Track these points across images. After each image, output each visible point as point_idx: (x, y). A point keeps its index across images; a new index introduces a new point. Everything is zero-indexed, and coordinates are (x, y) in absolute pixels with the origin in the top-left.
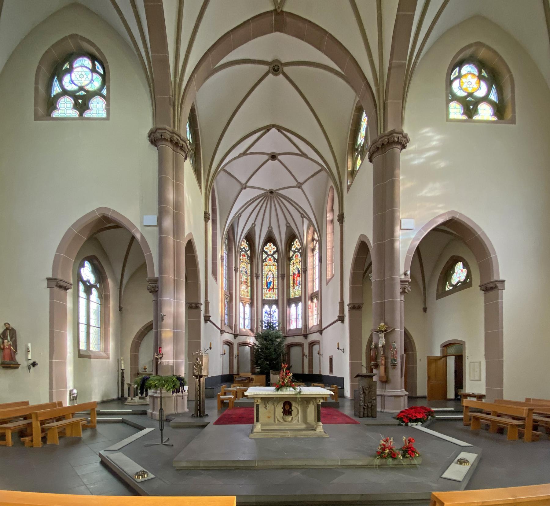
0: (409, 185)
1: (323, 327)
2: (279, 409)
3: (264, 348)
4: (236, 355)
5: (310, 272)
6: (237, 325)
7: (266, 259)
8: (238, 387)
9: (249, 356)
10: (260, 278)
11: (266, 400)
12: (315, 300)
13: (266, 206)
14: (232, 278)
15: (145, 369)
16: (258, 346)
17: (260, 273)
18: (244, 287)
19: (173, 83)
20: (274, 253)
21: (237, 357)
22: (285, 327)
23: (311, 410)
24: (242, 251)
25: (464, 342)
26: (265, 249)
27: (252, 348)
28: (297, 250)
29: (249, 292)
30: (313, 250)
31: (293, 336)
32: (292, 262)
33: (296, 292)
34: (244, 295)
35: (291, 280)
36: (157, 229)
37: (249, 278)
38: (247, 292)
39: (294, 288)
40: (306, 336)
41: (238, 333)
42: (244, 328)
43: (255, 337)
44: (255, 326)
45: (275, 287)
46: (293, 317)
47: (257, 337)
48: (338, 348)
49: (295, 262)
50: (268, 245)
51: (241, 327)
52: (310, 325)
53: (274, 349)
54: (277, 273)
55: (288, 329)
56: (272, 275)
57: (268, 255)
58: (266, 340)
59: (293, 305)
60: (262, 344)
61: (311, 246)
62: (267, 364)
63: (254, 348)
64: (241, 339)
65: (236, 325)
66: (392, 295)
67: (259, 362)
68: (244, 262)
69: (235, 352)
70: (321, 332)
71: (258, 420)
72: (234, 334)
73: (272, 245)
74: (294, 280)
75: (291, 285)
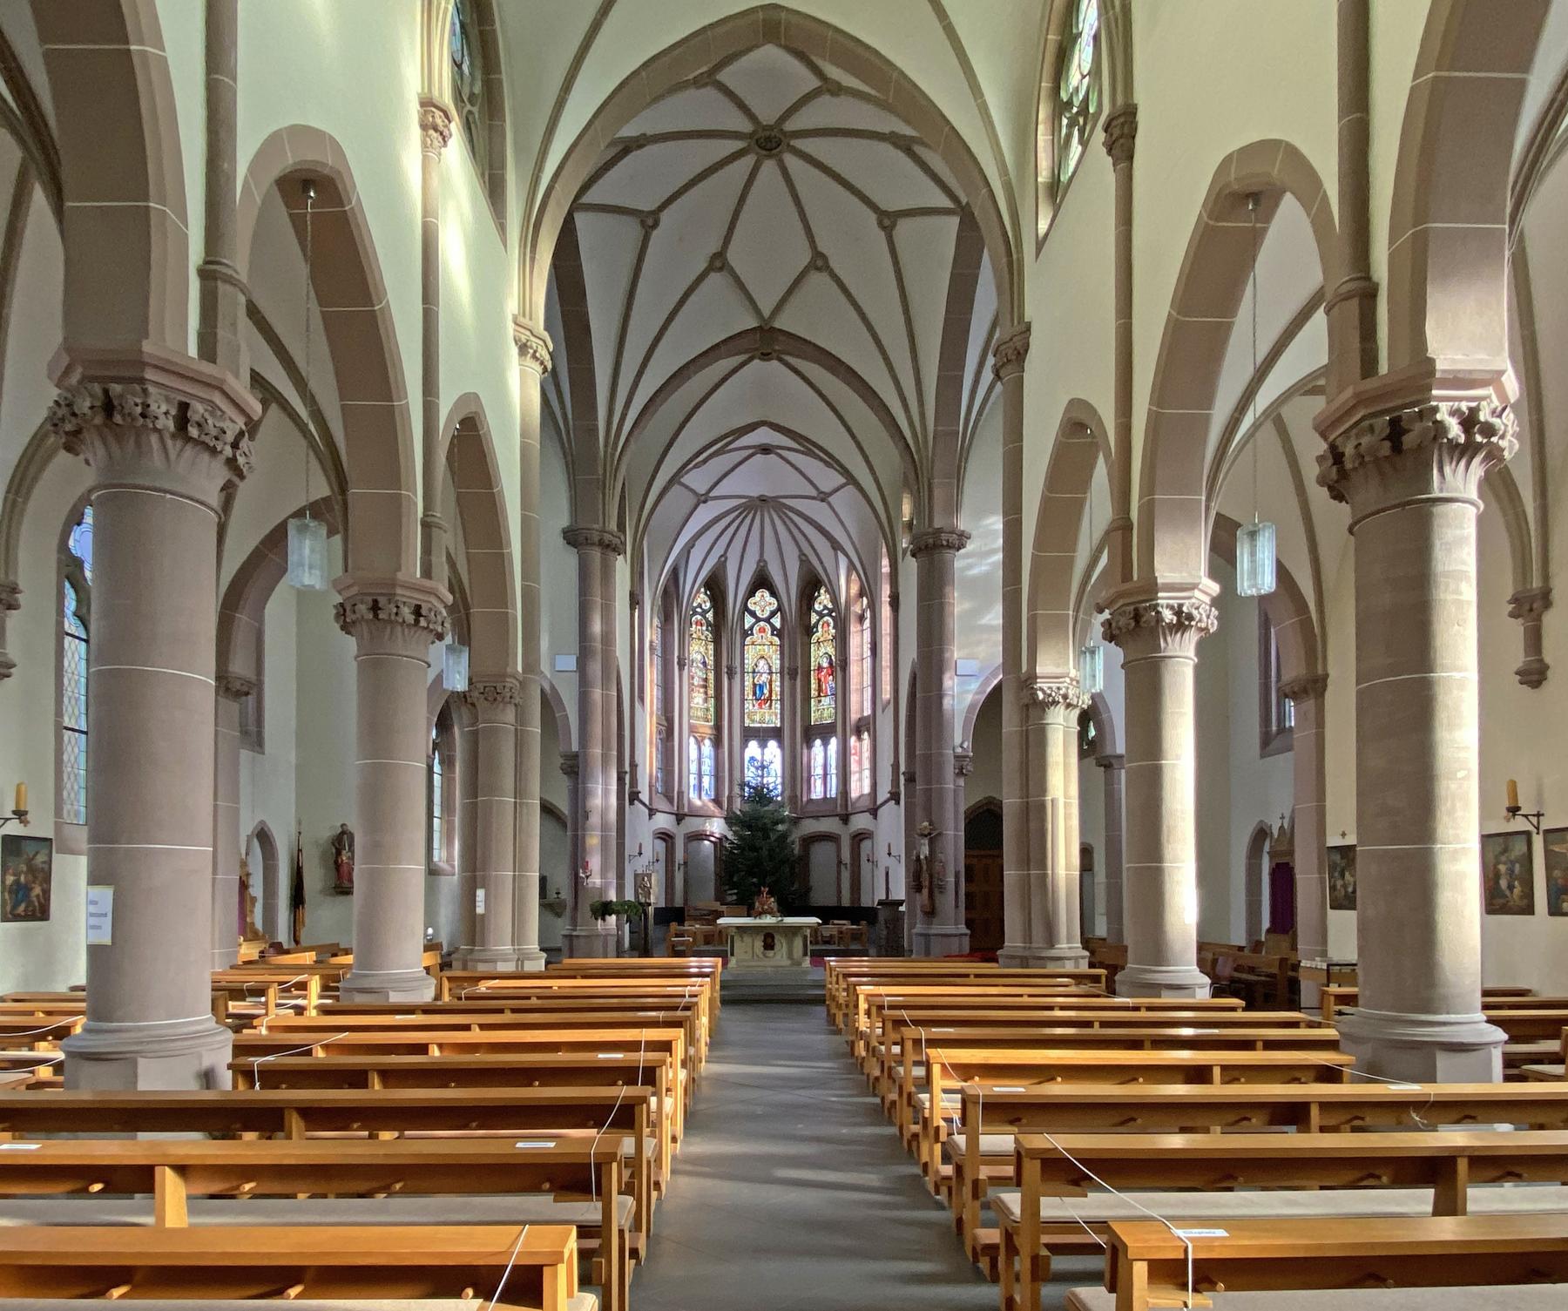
0: (967, 605)
1: (879, 802)
2: (759, 944)
3: (746, 846)
4: (682, 862)
5: (854, 669)
6: (683, 792)
7: (751, 628)
8: (697, 926)
9: (712, 868)
10: (737, 678)
11: (742, 929)
12: (866, 736)
13: (753, 521)
14: (673, 683)
15: (558, 893)
16: (733, 843)
17: (737, 663)
18: (698, 698)
19: (602, 453)
20: (773, 614)
21: (682, 868)
22: (799, 794)
23: (798, 943)
24: (695, 613)
25: (1261, 821)
26: (749, 605)
27: (719, 843)
28: (826, 612)
29: (712, 709)
30: (861, 618)
31: (817, 817)
32: (814, 639)
33: (823, 710)
34: (698, 718)
35: (813, 681)
36: (576, 677)
37: (711, 676)
38: (707, 710)
39: (820, 701)
40: (845, 819)
41: (686, 810)
42: (700, 798)
43: (725, 818)
44: (727, 794)
45: (774, 698)
46: (818, 770)
47: (730, 820)
48: (889, 854)
49: (821, 639)
50: (758, 594)
51: (693, 796)
52: (854, 794)
53: (769, 850)
54: (778, 662)
55: (805, 799)
56: (766, 667)
57: (758, 620)
58: (749, 828)
59: (818, 742)
60: (741, 838)
61: (856, 609)
62: (754, 883)
63: (722, 846)
64: (692, 825)
65: (680, 793)
66: (941, 780)
67: (735, 879)
68: (699, 639)
69: (679, 856)
70: (874, 812)
71: (732, 954)
72: (676, 815)
73: (767, 594)
74: (819, 680)
75: (814, 693)
